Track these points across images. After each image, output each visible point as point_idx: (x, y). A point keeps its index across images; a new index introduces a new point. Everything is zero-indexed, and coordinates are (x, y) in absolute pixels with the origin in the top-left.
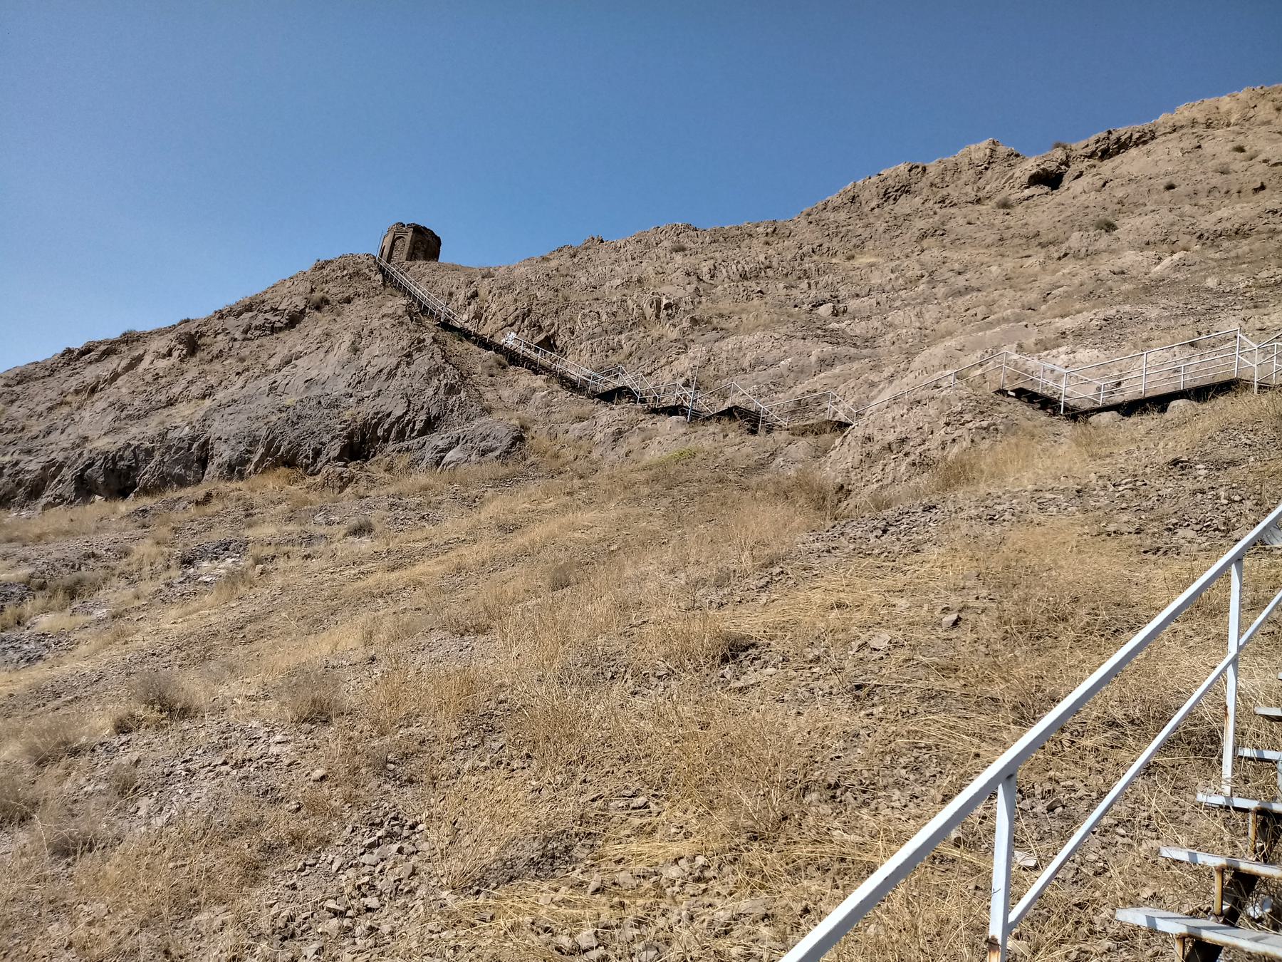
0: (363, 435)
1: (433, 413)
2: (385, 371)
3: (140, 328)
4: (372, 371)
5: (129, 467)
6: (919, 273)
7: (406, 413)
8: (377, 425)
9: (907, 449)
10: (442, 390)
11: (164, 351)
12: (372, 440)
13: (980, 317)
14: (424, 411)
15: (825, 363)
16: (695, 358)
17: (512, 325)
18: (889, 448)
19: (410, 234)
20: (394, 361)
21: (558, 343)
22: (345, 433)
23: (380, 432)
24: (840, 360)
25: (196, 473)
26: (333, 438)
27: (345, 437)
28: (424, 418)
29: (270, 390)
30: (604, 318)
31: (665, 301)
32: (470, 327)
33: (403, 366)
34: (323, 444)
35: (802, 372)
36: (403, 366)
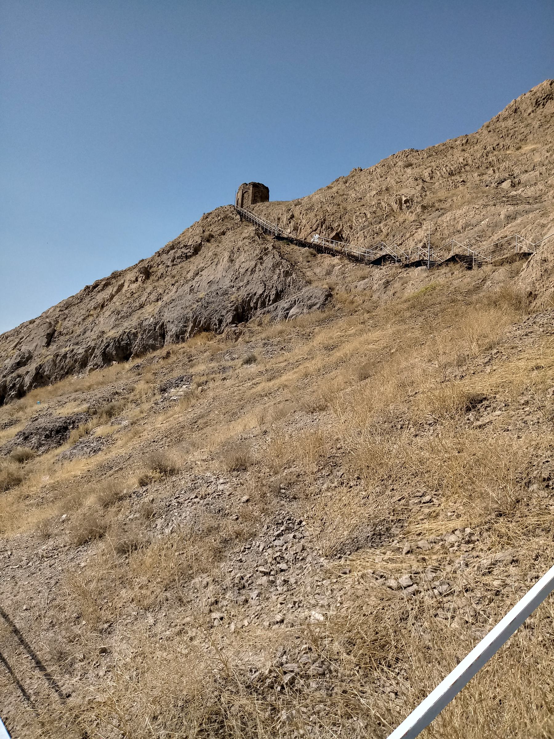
0: (243, 308)
2: (250, 270)
4: (242, 271)
5: (126, 344)
7: (264, 291)
8: (250, 300)
10: (282, 275)
11: (134, 279)
12: (248, 310)
14: (274, 289)
15: (510, 218)
17: (315, 230)
19: (251, 189)
20: (253, 263)
21: (344, 236)
22: (233, 308)
23: (252, 305)
25: (160, 342)
26: (227, 312)
27: (234, 310)
28: (274, 292)
29: (190, 291)
31: (404, 199)
32: (292, 236)
33: (259, 265)
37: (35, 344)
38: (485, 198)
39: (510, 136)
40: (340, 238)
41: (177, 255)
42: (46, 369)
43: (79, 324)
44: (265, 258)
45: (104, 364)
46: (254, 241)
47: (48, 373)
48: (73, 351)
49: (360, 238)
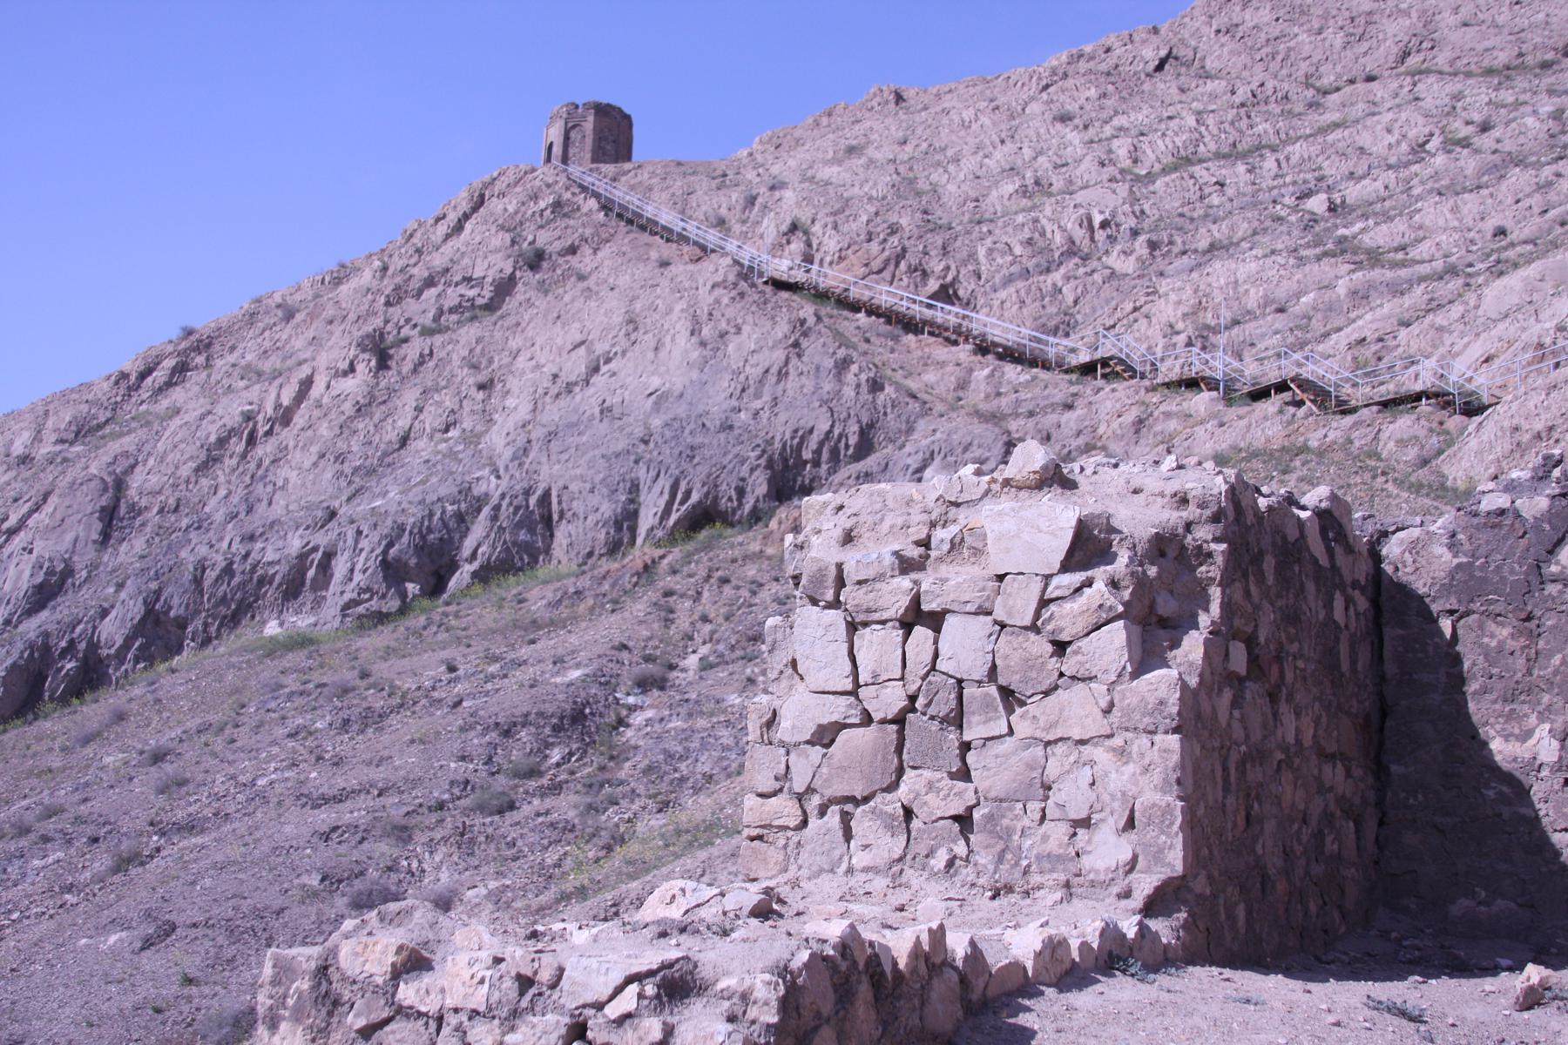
0: (785, 460)
1: (865, 420)
2: (774, 370)
3: (203, 322)
4: (753, 372)
5: (441, 539)
6: (1427, 130)
7: (832, 426)
8: (800, 444)
9: (1555, 435)
10: (864, 389)
11: (344, 365)
12: (796, 465)
13: (1536, 210)
14: (853, 420)
15: (1360, 296)
16: (1179, 302)
17: (880, 271)
18: (1538, 436)
19: (591, 118)
20: (779, 355)
21: (961, 293)
22: (763, 461)
23: (807, 455)
24: (1375, 289)
25: (543, 536)
26: (752, 470)
27: (766, 467)
28: (856, 428)
29: (602, 412)
30: (1018, 250)
31: (1098, 219)
32: (799, 276)
33: (794, 361)
34: (743, 480)
35: (1330, 310)
36: (794, 361)
37: (69, 537)
38: (1286, 238)
39: (1279, 58)
40: (948, 296)
41: (447, 304)
42: (176, 601)
43: (188, 482)
44: (804, 343)
45: (389, 588)
46: (742, 295)
47: (182, 611)
48: (247, 555)
49: (1008, 304)
